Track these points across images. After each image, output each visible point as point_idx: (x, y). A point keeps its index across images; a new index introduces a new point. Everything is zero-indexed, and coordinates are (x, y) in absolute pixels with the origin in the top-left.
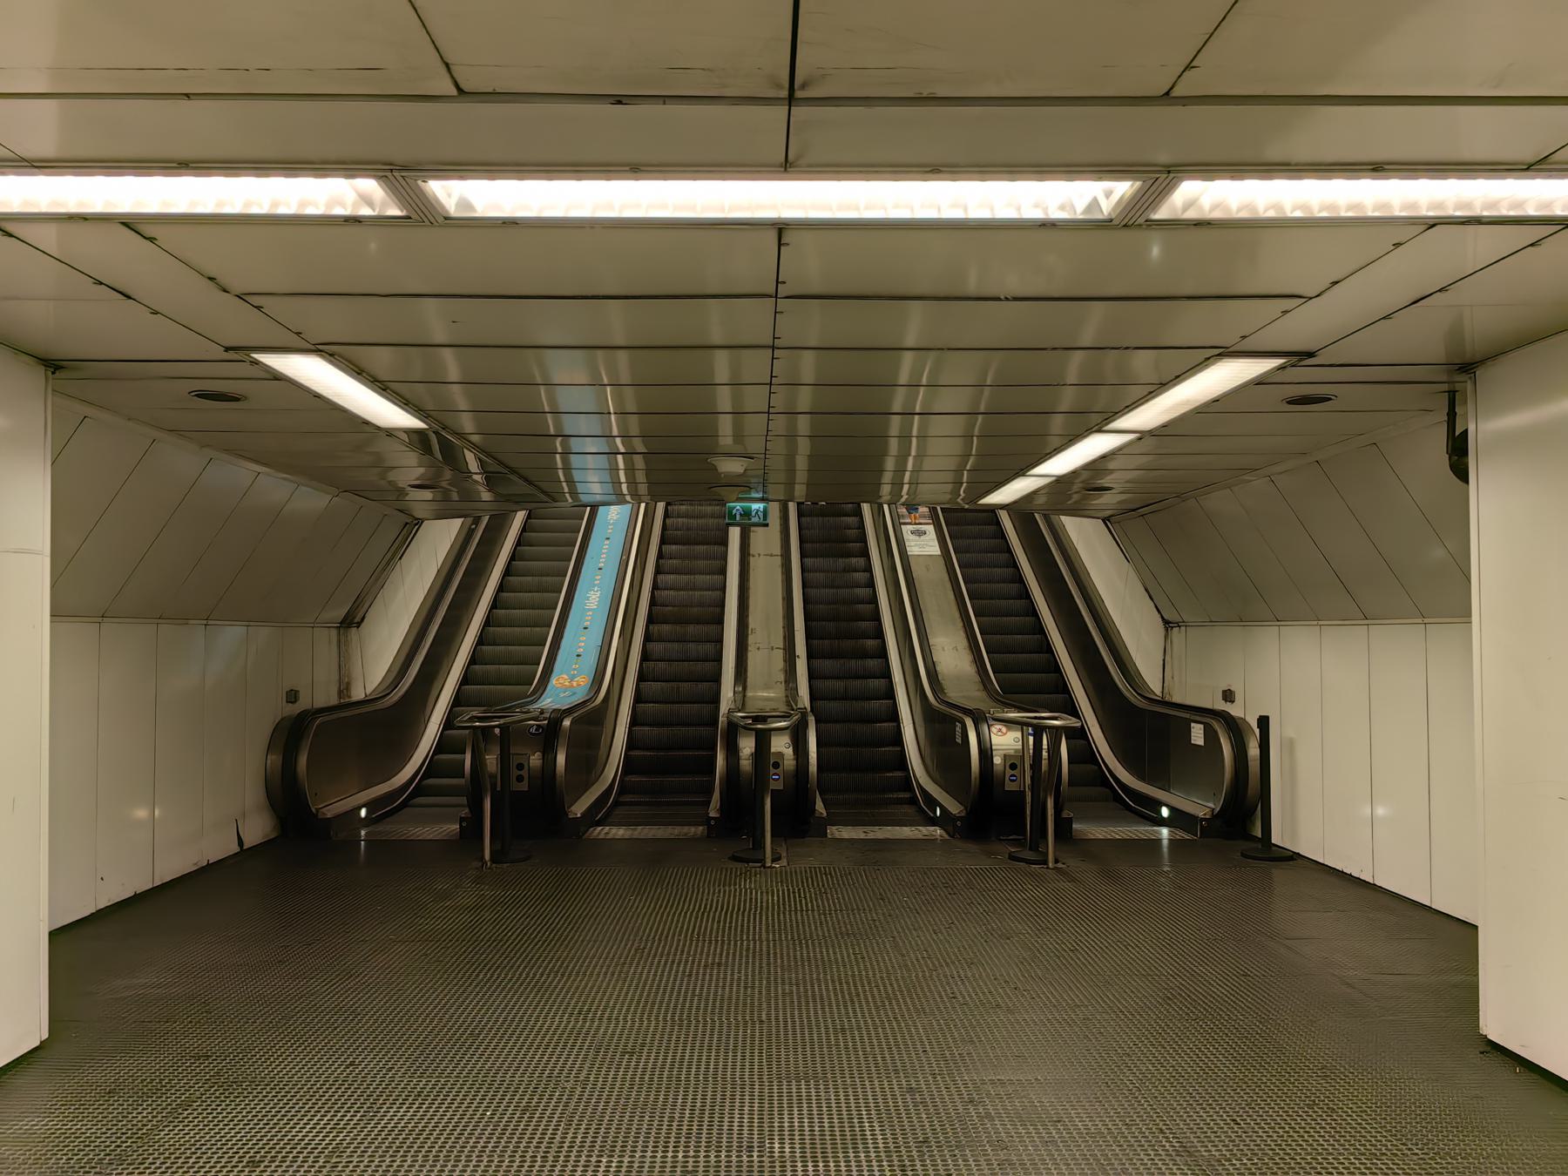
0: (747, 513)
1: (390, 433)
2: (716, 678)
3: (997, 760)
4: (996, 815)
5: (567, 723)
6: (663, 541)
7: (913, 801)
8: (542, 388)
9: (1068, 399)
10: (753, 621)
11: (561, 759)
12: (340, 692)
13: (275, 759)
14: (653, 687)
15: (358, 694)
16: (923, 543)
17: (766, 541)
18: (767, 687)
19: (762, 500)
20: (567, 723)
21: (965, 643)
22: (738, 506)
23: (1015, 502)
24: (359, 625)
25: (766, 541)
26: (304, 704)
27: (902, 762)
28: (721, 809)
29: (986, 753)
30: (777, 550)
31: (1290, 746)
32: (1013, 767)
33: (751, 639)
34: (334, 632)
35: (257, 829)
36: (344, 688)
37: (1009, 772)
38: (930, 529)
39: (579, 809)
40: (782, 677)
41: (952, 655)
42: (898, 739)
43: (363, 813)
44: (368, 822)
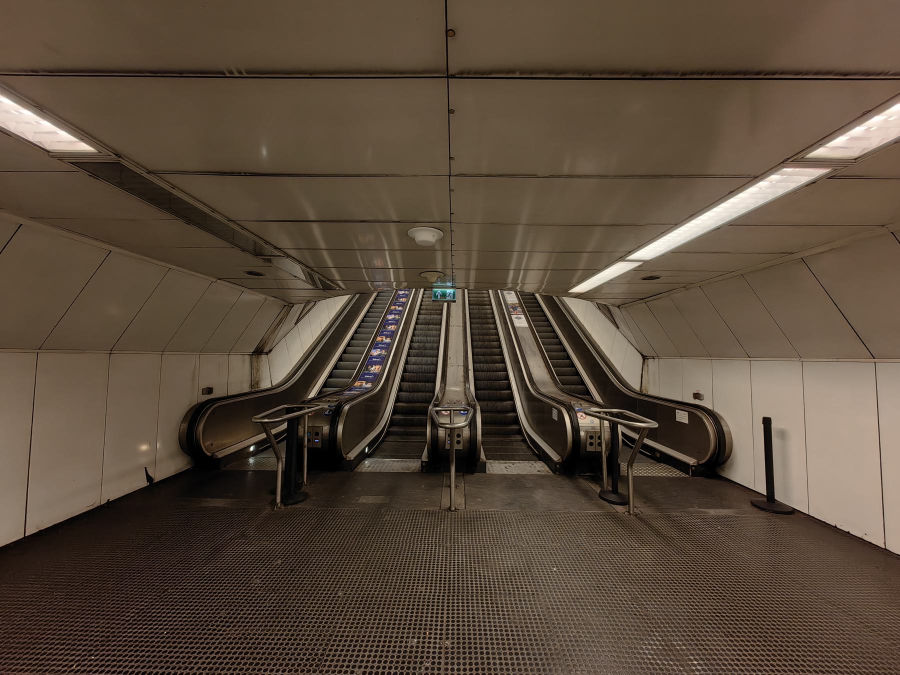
0: (444, 295)
1: (61, 157)
2: (434, 382)
3: (582, 434)
4: (579, 463)
5: (347, 407)
6: (416, 323)
7: (524, 441)
8: (358, 252)
9: (582, 265)
10: (450, 354)
11: (340, 428)
12: (251, 386)
13: (185, 426)
14: (406, 384)
15: (265, 384)
16: (521, 322)
17: (456, 309)
18: (456, 386)
19: (453, 287)
20: (347, 407)
21: (543, 364)
22: (439, 291)
23: (587, 292)
24: (267, 354)
25: (456, 309)
26: (217, 394)
27: (516, 421)
28: (429, 457)
29: (576, 428)
30: (461, 324)
31: (783, 434)
32: (591, 437)
33: (449, 361)
34: (247, 358)
35: (170, 465)
36: (255, 383)
37: (589, 441)
38: (523, 316)
39: (352, 455)
40: (462, 379)
41: (538, 370)
42: (514, 409)
43: (252, 449)
44: (253, 454)
